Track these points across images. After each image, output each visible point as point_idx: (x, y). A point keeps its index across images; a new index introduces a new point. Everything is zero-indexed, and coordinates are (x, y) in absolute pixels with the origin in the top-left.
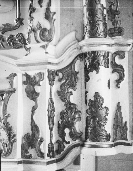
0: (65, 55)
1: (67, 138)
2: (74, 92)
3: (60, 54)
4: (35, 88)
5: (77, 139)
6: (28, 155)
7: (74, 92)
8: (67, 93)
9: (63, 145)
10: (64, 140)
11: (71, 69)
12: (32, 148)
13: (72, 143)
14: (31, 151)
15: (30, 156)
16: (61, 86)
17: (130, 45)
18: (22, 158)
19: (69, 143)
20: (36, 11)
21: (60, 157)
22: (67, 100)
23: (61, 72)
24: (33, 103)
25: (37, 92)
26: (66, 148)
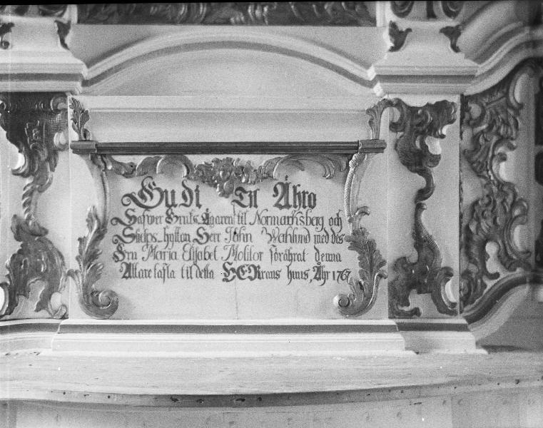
0: (497, 56)
1: (492, 266)
2: (510, 154)
3: (101, 183)
4: (426, 141)
5: (519, 266)
6: (406, 309)
7: (510, 154)
8: (493, 156)
9: (482, 281)
10: (484, 272)
11: (506, 95)
12: (419, 292)
13: (505, 275)
14: (417, 300)
15: (416, 312)
16: (475, 139)
17: (197, 186)
18: (390, 318)
19: (496, 275)
20: (10, 47)
21: (472, 312)
22: (492, 172)
23: (476, 103)
24: (420, 181)
25: (431, 152)
26: (488, 288)
